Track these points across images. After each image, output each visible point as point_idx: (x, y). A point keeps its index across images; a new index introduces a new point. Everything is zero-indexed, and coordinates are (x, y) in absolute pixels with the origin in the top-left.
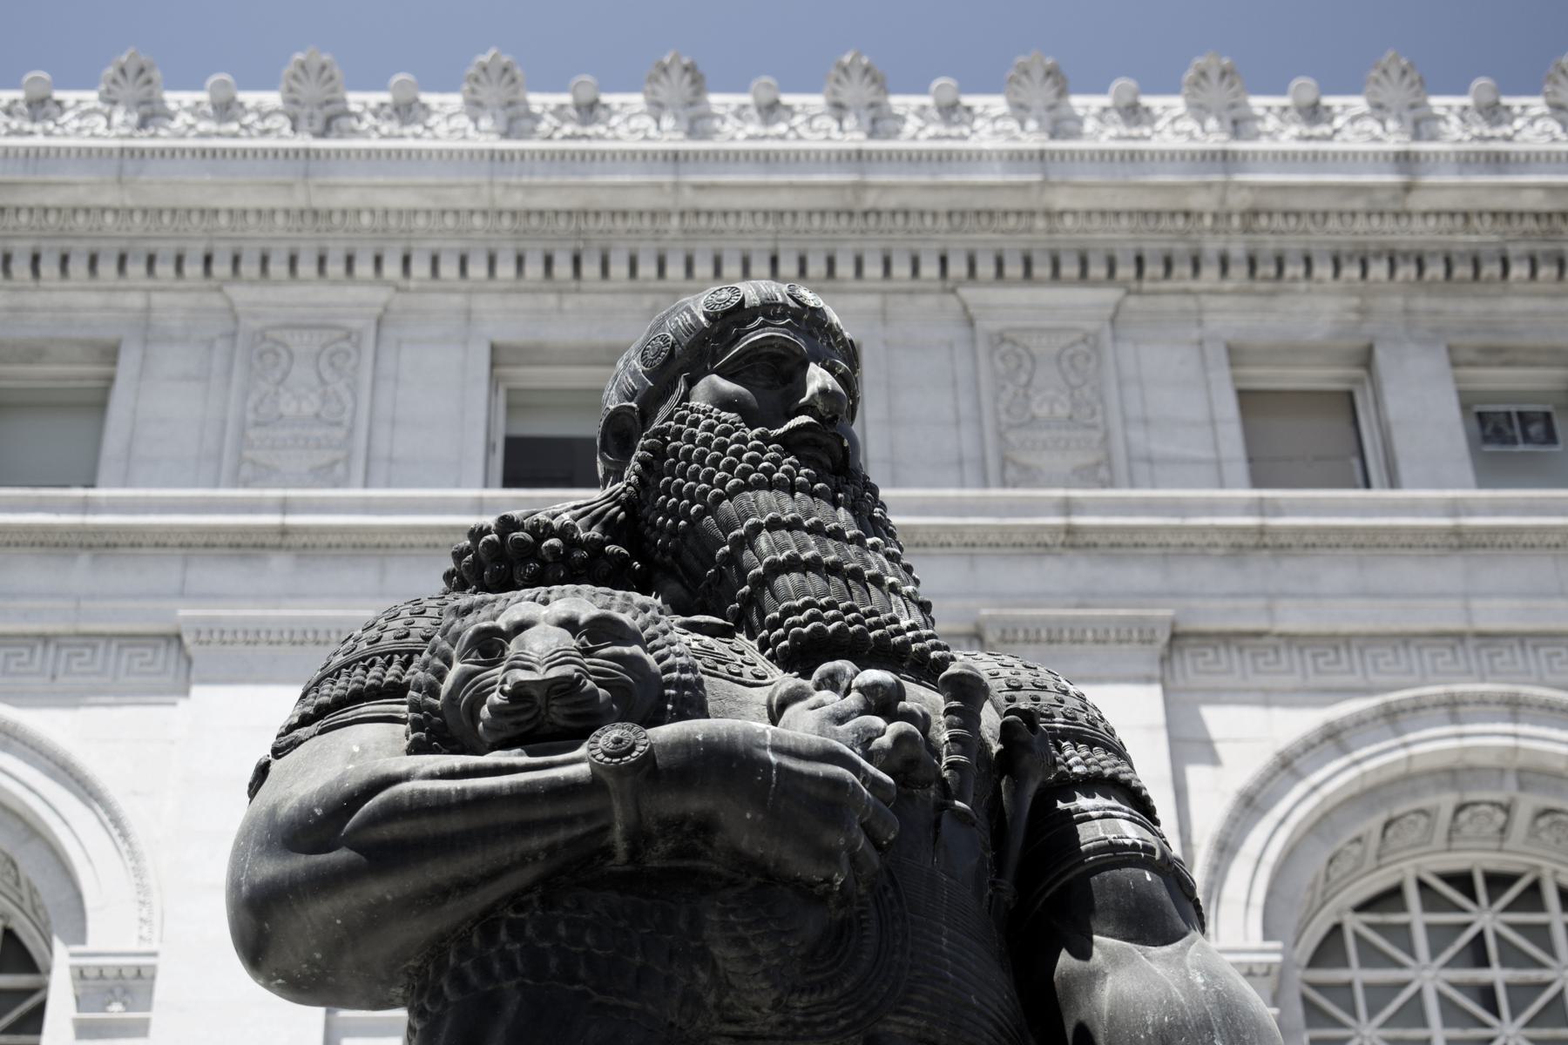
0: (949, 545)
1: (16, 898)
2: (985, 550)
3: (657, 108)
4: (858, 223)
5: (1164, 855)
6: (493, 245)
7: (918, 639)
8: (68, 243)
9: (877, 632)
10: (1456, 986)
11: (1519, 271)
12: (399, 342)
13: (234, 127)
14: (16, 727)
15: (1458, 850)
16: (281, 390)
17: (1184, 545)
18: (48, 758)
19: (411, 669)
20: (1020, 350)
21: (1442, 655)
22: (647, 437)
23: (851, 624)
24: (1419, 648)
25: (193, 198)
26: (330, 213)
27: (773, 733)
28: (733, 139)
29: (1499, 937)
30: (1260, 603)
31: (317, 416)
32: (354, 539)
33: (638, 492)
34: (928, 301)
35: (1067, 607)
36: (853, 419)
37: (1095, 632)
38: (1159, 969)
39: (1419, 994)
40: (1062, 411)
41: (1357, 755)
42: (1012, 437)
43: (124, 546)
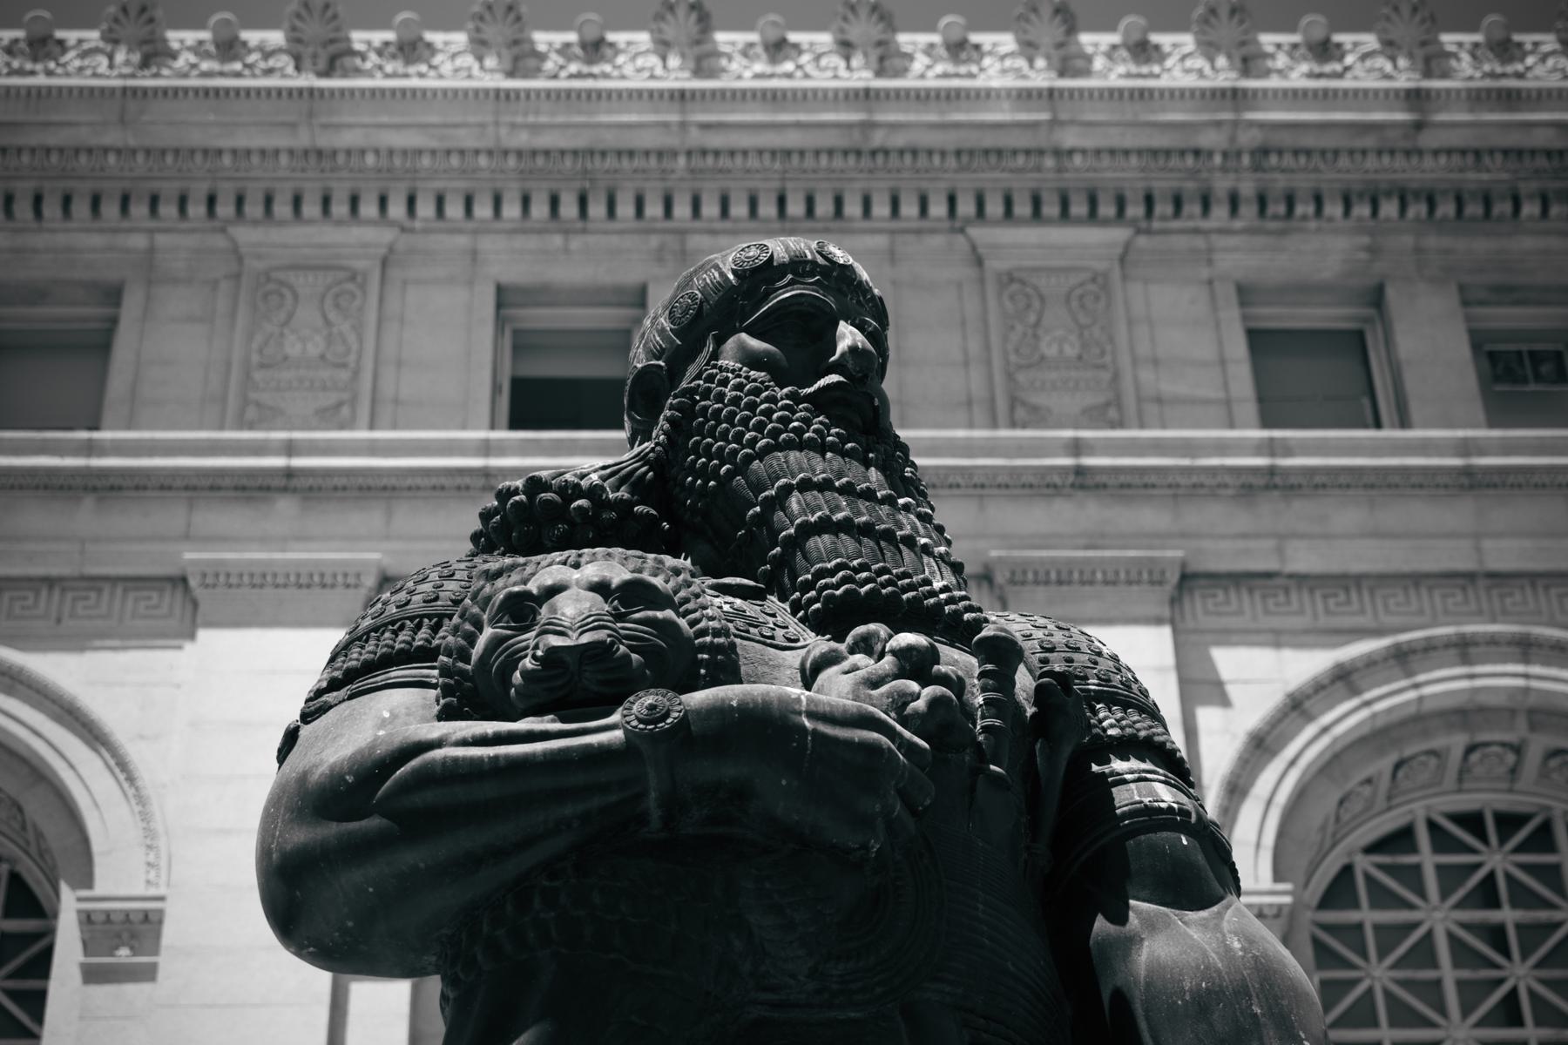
0: (958, 486)
1: (22, 842)
2: (996, 491)
3: (663, 47)
4: (865, 162)
5: (1200, 818)
6: (499, 185)
7: (951, 601)
8: (70, 184)
9: (911, 594)
10: (1466, 926)
11: (1530, 209)
12: (405, 283)
13: (238, 66)
14: (21, 670)
15: (1469, 791)
16: (286, 331)
17: (1194, 486)
18: (54, 701)
19: (441, 634)
20: (1028, 290)
21: (1453, 595)
22: (675, 397)
23: (884, 586)
24: (1430, 589)
25: (196, 138)
26: (334, 153)
27: (808, 698)
28: (739, 77)
29: (1509, 878)
30: (1270, 543)
31: (322, 357)
32: (360, 481)
33: (666, 451)
34: (937, 241)
35: (1077, 548)
36: (882, 377)
37: (1104, 573)
38: (1195, 934)
39: (1429, 934)
40: (1071, 351)
41: (1368, 696)
42: (1021, 377)
43: (128, 488)
